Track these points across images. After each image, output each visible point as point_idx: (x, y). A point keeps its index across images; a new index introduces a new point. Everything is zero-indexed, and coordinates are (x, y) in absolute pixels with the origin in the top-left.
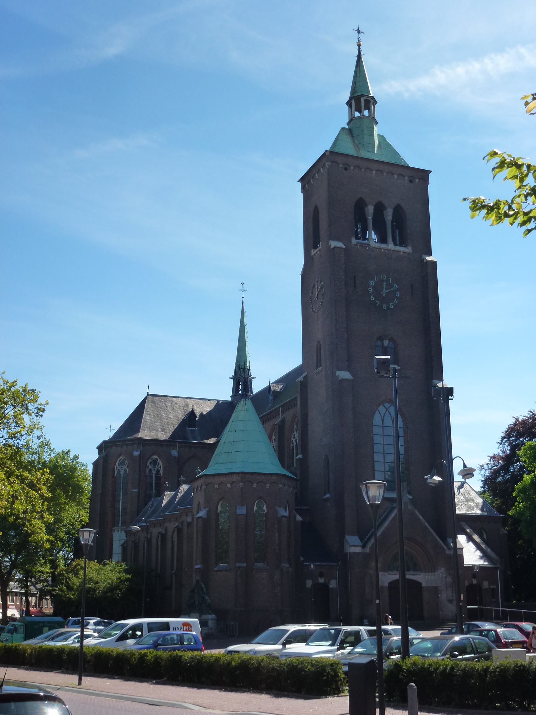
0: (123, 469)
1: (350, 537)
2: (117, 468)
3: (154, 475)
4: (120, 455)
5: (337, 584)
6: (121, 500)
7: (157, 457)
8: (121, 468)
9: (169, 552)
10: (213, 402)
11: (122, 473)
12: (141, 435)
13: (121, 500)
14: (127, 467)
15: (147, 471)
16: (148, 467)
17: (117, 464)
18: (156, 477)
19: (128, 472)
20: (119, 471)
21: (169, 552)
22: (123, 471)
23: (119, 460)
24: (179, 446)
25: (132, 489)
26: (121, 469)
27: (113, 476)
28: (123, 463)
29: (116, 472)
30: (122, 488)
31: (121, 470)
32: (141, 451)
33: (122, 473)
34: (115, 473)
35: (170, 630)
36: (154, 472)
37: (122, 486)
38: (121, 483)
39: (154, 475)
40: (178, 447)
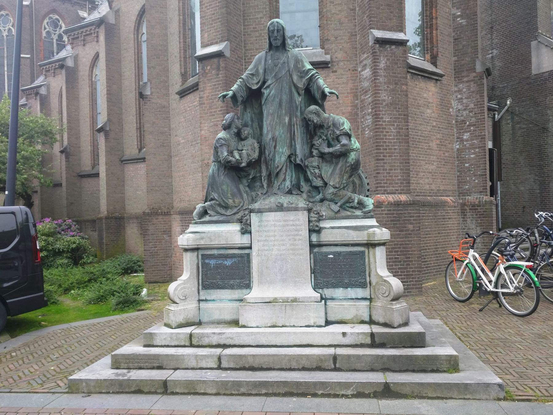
0: (6, 28)
3: (55, 41)
5: (226, 248)
6: (6, 73)
7: (58, 17)
9: (85, 103)
13: (6, 73)
15: (44, 34)
16: (45, 29)
18: (58, 44)
21: (85, 103)
22: (6, 31)
24: (90, 6)
35: (248, 286)
36: (55, 38)
37: (6, 52)
38: (4, 49)
39: (55, 41)
40: (89, 8)
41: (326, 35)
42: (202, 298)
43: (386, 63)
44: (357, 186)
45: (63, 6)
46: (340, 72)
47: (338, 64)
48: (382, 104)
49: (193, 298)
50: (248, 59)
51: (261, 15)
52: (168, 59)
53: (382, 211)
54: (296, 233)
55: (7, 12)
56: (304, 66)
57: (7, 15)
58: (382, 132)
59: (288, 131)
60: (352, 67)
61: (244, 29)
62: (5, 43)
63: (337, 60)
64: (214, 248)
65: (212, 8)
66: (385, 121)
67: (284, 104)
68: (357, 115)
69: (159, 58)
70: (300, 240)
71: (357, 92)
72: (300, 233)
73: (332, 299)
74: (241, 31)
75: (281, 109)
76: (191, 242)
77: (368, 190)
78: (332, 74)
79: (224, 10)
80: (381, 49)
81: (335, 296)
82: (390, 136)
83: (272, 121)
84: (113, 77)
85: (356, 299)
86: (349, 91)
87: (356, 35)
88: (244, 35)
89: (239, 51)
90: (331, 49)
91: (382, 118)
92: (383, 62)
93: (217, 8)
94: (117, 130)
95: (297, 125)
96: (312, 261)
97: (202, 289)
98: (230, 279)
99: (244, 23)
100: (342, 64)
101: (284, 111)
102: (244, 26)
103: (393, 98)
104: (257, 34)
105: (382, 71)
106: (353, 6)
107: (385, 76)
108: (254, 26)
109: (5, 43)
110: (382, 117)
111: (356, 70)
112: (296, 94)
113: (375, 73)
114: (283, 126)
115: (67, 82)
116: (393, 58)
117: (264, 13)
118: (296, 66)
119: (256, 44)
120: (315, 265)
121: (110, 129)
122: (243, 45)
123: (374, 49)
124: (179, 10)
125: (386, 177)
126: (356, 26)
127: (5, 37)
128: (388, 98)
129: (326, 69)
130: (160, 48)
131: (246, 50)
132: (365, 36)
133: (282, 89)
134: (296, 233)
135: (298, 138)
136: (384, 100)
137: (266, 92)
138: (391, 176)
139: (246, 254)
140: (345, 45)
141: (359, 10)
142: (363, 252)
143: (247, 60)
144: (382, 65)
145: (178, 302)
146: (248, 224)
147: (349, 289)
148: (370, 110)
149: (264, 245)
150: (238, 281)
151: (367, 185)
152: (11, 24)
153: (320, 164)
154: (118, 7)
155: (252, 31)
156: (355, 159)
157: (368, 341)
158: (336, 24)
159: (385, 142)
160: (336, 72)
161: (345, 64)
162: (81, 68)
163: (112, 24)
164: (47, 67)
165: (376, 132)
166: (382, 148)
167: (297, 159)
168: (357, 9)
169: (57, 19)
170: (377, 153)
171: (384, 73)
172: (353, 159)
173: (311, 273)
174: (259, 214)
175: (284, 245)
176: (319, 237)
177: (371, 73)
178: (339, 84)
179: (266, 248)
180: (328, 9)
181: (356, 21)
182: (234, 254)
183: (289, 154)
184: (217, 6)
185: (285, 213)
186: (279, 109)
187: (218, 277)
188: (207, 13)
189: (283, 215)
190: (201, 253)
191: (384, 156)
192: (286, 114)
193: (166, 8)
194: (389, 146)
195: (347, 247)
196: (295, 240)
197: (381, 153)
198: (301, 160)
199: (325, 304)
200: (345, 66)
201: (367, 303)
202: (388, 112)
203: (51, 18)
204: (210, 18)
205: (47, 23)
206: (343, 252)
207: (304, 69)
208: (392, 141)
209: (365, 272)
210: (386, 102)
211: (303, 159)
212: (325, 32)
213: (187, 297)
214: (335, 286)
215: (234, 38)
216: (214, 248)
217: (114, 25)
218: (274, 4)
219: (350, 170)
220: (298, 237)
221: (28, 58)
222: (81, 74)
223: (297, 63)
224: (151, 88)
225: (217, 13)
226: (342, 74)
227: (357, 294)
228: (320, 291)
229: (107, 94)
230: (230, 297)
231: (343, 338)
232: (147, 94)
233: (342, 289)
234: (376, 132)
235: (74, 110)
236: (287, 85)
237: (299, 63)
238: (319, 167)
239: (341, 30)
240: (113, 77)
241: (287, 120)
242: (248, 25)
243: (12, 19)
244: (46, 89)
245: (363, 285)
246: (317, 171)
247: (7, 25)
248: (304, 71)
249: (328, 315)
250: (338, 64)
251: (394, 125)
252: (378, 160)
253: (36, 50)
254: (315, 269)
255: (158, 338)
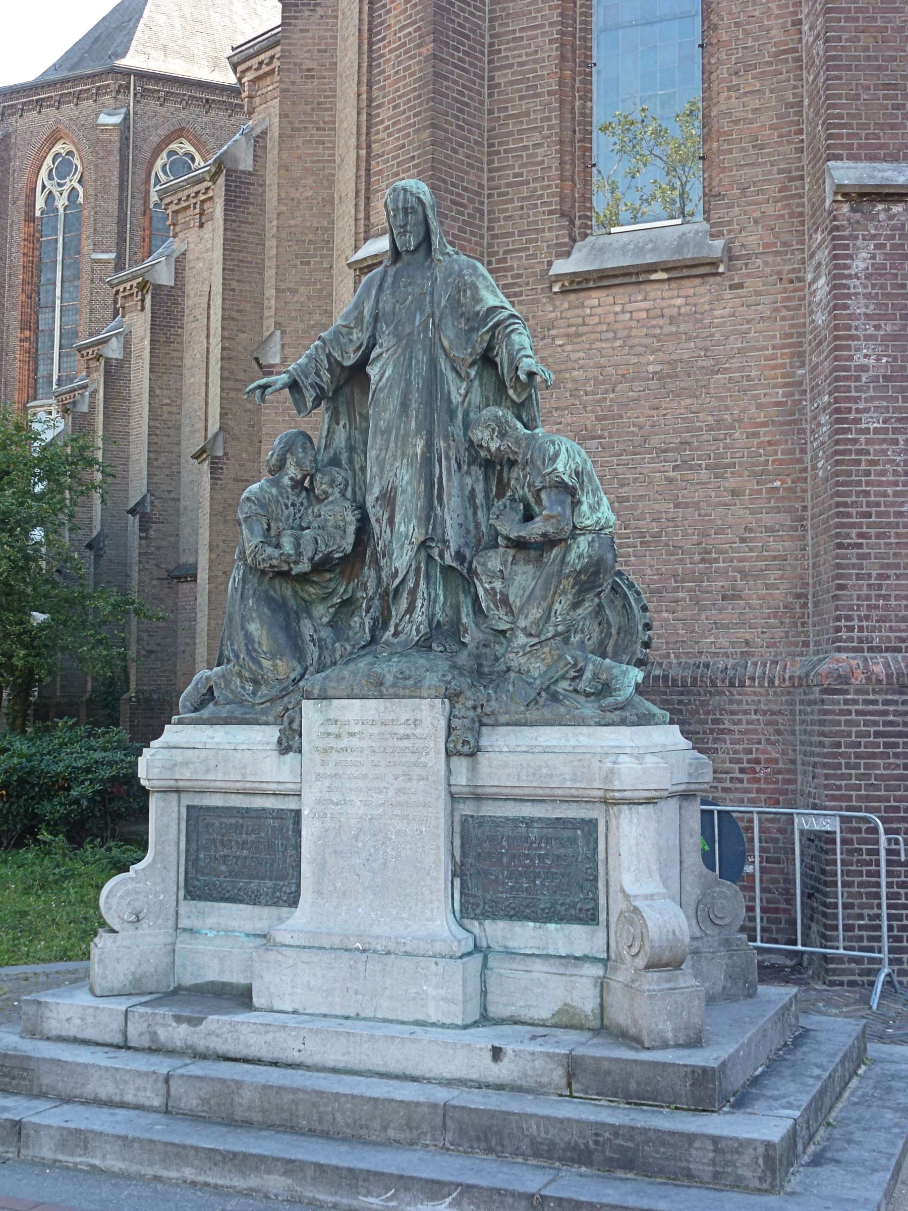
0: (65, 188)
1: (131, 493)
2: (44, 187)
4: (54, 138)
7: (192, 149)
8: (60, 185)
10: (182, 911)
11: (61, 202)
12: (132, 60)
14: (79, 182)
17: (43, 173)
19: (81, 200)
20: (50, 197)
22: (66, 194)
23: (49, 160)
25: (94, 251)
26: (56, 191)
27: (30, 218)
28: (63, 168)
29: (40, 203)
30: (60, 258)
31: (57, 194)
32: (127, 114)
33: (61, 202)
34: (38, 207)
35: (293, 901)
38: (56, 240)
41: (715, 183)
42: (184, 923)
43: (873, 257)
44: (614, 631)
45: (205, 119)
46: (752, 285)
47: (746, 265)
48: (858, 379)
49: (160, 921)
50: (499, 261)
51: (537, 138)
52: (331, 267)
53: (846, 702)
54: (414, 758)
55: (70, 147)
56: (477, 300)
57: (70, 153)
58: (858, 462)
59: (420, 475)
60: (789, 272)
61: (491, 179)
62: (60, 227)
63: (744, 252)
64: (264, 794)
65: (400, 130)
66: (866, 431)
67: (414, 405)
68: (802, 411)
69: (308, 263)
70: (422, 779)
71: (800, 344)
72: (423, 759)
73: (509, 953)
74: (481, 186)
75: (407, 416)
76: (156, 770)
77: (646, 645)
78: (728, 294)
79: (425, 135)
80: (858, 216)
81: (512, 944)
82: (883, 473)
83: (384, 452)
84: (240, 311)
85: (567, 957)
86: (778, 341)
87: (802, 178)
88: (490, 196)
89: (470, 241)
90: (730, 223)
91: (857, 421)
92: (864, 255)
93: (411, 130)
94: (244, 455)
95: (448, 458)
96: (457, 842)
97: (185, 898)
98: (252, 877)
99: (491, 162)
100: (759, 262)
101: (413, 424)
102: (490, 171)
103: (895, 359)
104: (525, 191)
105: (858, 283)
106: (795, 95)
107: (867, 296)
108: (517, 170)
109: (60, 227)
110: (855, 418)
111: (801, 280)
112: (450, 375)
113: (837, 286)
114: (410, 464)
115: (154, 326)
116: (897, 241)
117: (545, 132)
118: (455, 304)
119: (521, 217)
120: (464, 854)
121: (226, 454)
122: (486, 224)
123: (835, 218)
124: (358, 133)
125: (868, 598)
126: (801, 150)
127: (61, 211)
128: (878, 359)
129: (712, 280)
130: (311, 236)
131: (494, 237)
132: (819, 180)
133: (410, 365)
134: (414, 758)
135: (450, 496)
136: (864, 368)
137: (373, 371)
138: (886, 597)
139: (292, 811)
140: (770, 209)
141: (809, 105)
142: (592, 824)
143: (494, 266)
144: (859, 265)
145: (116, 928)
146: (294, 731)
147: (552, 926)
148: (826, 398)
149: (330, 789)
150: (269, 883)
151: (640, 628)
152: (78, 175)
153: (506, 567)
154: (264, 127)
155: (508, 185)
156: (590, 557)
157: (558, 1076)
158: (743, 150)
159: (867, 494)
160: (740, 286)
161: (766, 264)
162: (192, 287)
163: (243, 172)
164: (128, 285)
165: (838, 463)
166: (853, 511)
167: (447, 556)
168: (806, 102)
169: (187, 154)
170: (838, 525)
171: (865, 287)
172: (580, 557)
173: (454, 875)
174: (325, 702)
175: (381, 792)
176: (473, 769)
177: (828, 289)
178: (748, 322)
179: (336, 797)
180: (723, 107)
181: (804, 137)
182: (264, 809)
183: (422, 538)
184: (410, 126)
185: (388, 703)
186: (400, 417)
187: (223, 868)
188: (388, 144)
189: (382, 708)
190: (187, 800)
191: (861, 535)
192: (418, 431)
193: (334, 129)
194: (878, 504)
195: (549, 807)
196: (410, 779)
197: (852, 525)
198: (459, 556)
199: (485, 965)
200: (768, 270)
201: (597, 971)
202: (876, 404)
203: (172, 153)
204: (394, 158)
205: (164, 167)
206: (540, 819)
207: (477, 308)
208: (890, 491)
209: (596, 879)
210: (871, 373)
211: (468, 553)
212: (714, 174)
213: (141, 916)
214: (518, 915)
215: (454, 207)
216: (264, 794)
217: (250, 174)
218: (577, 103)
219: (573, 587)
220: (418, 771)
221: (108, 262)
222: (189, 302)
223: (459, 292)
224: (283, 346)
225: (411, 143)
226: (757, 293)
227: (571, 943)
228: (475, 926)
229: (222, 359)
230: (249, 927)
231: (493, 1065)
232: (272, 362)
233: (531, 924)
234: (838, 463)
235: (168, 401)
236: (424, 353)
237: (465, 291)
238: (502, 576)
239: (759, 165)
240: (240, 311)
241: (420, 445)
242: (498, 169)
243: (79, 164)
244: (121, 345)
245: (589, 917)
246: (498, 585)
247: (67, 180)
248: (478, 313)
249: (490, 997)
250: (746, 265)
251: (896, 442)
252: (840, 546)
253: (131, 239)
254: (462, 864)
255: (55, 1015)
